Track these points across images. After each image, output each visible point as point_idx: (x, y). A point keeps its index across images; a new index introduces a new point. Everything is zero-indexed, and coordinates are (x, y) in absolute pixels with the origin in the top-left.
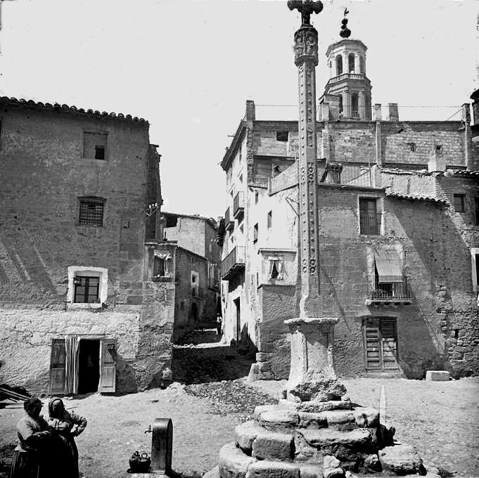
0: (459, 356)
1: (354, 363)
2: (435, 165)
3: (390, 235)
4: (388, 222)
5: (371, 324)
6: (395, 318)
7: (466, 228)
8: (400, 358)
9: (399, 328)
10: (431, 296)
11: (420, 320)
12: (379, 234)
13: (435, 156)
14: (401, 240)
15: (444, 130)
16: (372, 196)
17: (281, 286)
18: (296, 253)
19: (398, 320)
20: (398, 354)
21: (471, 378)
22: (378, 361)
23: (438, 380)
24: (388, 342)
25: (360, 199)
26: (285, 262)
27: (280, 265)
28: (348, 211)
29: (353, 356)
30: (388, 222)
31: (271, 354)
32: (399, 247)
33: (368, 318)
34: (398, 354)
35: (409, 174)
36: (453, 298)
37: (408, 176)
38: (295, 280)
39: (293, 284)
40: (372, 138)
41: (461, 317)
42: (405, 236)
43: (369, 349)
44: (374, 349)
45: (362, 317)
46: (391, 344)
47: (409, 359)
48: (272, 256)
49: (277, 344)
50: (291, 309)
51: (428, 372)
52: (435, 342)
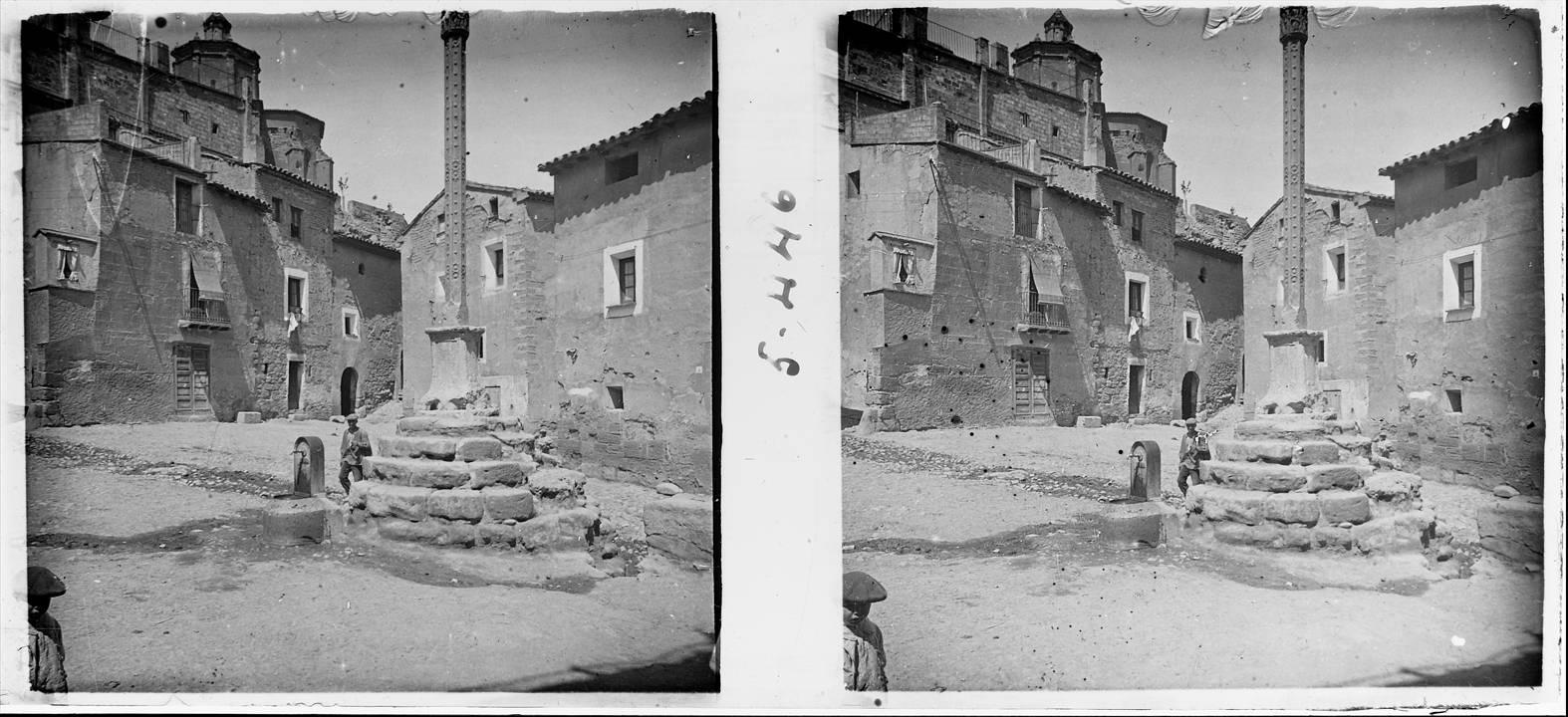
0: (268, 394)
1: (1001, 407)
2: (255, 155)
3: (208, 238)
4: (1045, 224)
5: (182, 353)
6: (208, 347)
7: (281, 242)
8: (212, 397)
9: (212, 359)
10: (246, 322)
11: (1073, 355)
12: (195, 234)
13: (255, 142)
14: (220, 245)
15: (223, 105)
16: (1030, 183)
17: (76, 291)
18: (933, 247)
19: (211, 348)
20: (1049, 397)
21: (1116, 424)
22: (189, 401)
23: (251, 422)
24: (199, 376)
25: (177, 182)
26: (81, 256)
27: (74, 260)
28: (1001, 199)
29: (161, 393)
30: (1045, 224)
31: (896, 394)
32: (1057, 258)
33: (180, 343)
34: (1049, 397)
35: (214, 158)
36: (266, 326)
37: (1051, 163)
38: (95, 284)
39: (927, 293)
40: (974, 90)
41: (1112, 353)
42: (1064, 245)
43: (179, 385)
44: (185, 385)
45: (174, 342)
46: (204, 379)
47: (221, 398)
48: (899, 247)
49: (69, 375)
50: (88, 325)
51: (1079, 417)
52: (1087, 381)
